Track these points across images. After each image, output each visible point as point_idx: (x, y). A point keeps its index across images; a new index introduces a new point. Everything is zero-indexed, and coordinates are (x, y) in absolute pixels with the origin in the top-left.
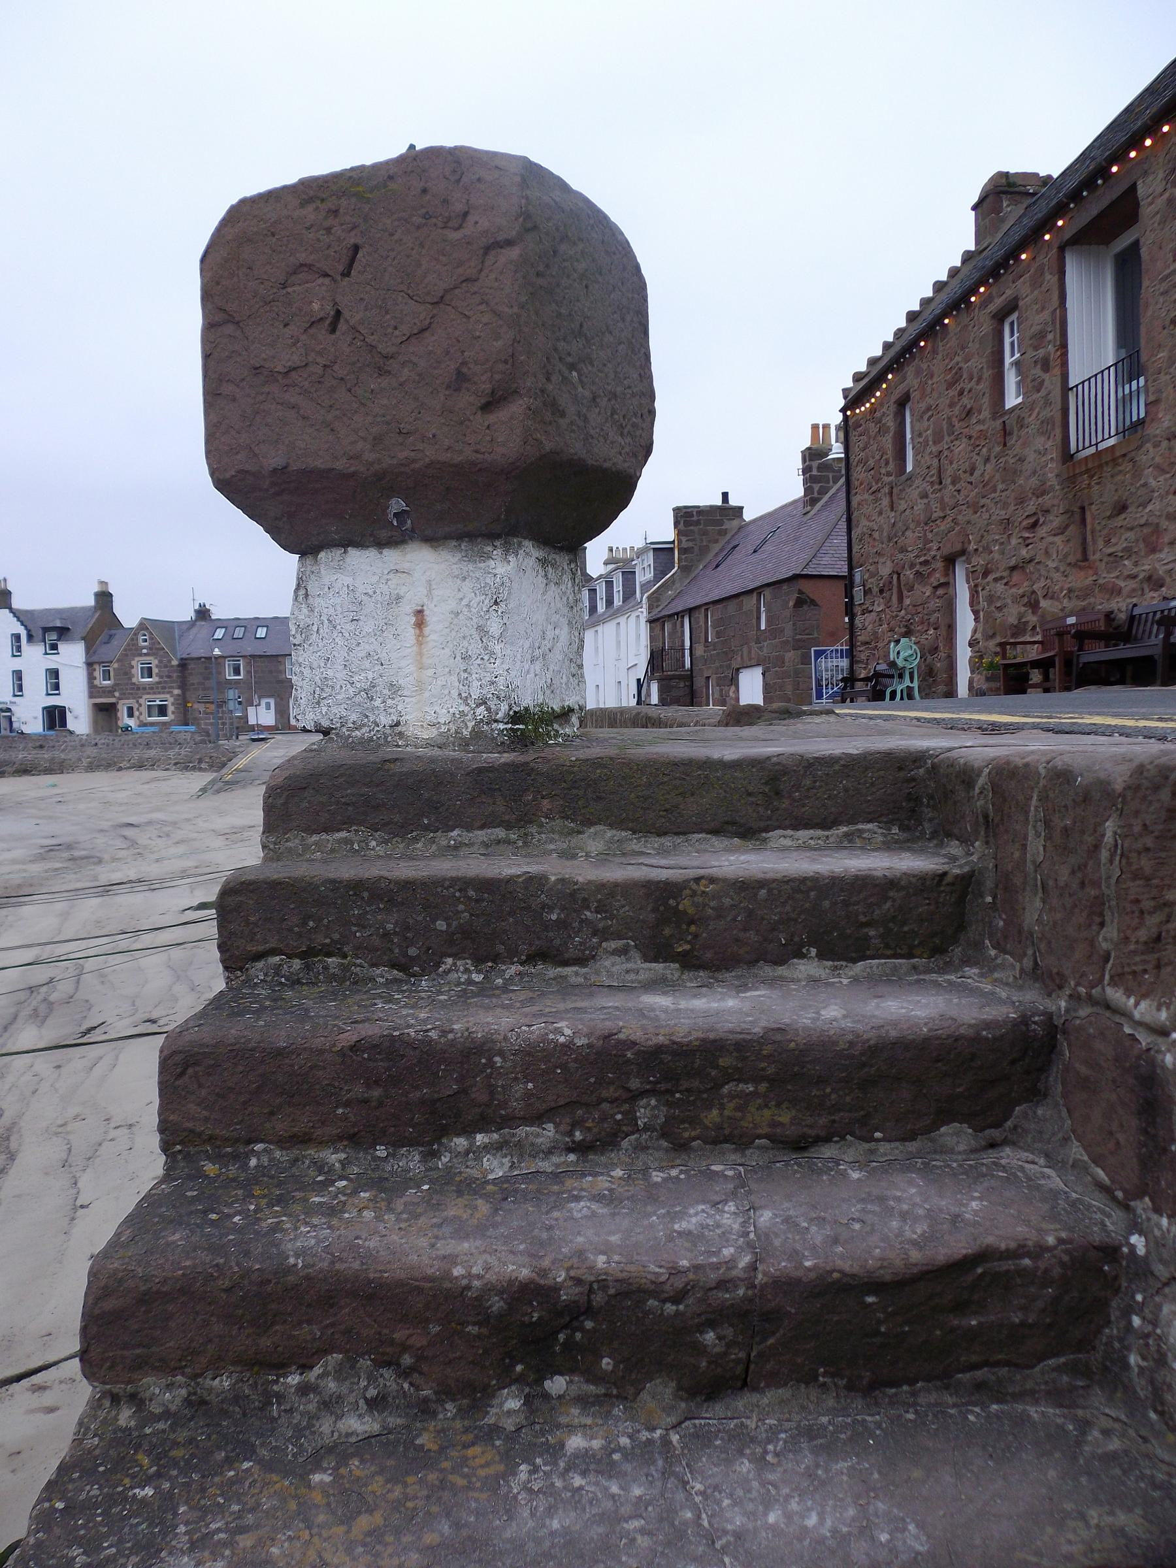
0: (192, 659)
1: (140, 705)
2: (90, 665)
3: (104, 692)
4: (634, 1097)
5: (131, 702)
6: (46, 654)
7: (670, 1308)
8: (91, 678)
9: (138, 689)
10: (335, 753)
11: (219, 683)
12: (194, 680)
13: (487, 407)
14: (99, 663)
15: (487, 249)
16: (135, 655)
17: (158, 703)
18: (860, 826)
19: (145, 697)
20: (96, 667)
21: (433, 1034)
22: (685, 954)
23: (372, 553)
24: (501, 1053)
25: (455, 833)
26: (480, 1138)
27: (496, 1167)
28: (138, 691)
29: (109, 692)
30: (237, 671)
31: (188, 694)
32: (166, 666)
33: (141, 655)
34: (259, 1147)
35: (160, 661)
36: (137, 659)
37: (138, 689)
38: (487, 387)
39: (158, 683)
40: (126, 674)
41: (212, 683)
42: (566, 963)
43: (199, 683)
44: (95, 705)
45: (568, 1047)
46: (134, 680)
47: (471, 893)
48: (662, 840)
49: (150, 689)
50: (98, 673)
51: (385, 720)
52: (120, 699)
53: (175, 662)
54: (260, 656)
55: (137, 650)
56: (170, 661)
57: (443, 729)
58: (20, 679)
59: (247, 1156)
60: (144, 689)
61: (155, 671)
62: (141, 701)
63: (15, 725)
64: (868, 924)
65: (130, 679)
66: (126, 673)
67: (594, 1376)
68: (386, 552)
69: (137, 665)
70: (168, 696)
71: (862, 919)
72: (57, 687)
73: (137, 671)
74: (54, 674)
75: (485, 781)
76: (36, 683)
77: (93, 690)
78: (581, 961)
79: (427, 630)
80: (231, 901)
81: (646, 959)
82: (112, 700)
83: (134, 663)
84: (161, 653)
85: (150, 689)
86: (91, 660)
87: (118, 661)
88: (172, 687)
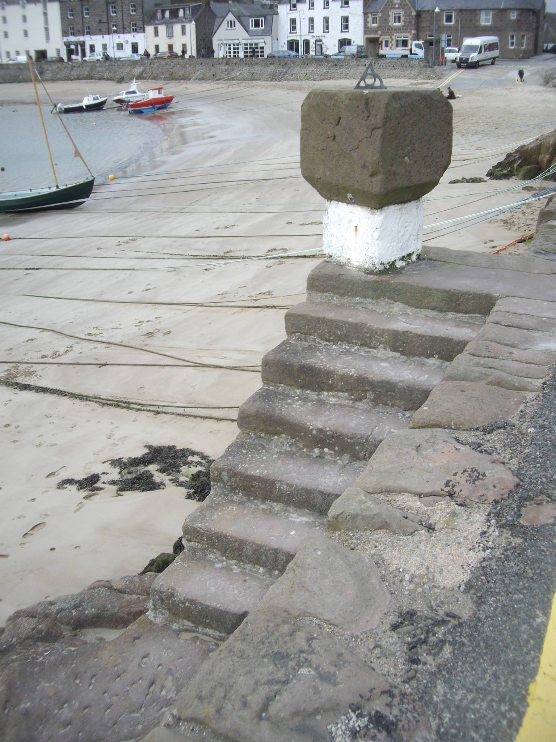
0: (424, 11)
1: (392, 40)
2: (365, 14)
3: (373, 31)
4: (366, 391)
5: (387, 38)
6: (342, 7)
7: (349, 441)
8: (366, 22)
9: (392, 29)
10: (328, 270)
11: (439, 27)
12: (424, 24)
13: (371, 176)
14: (371, 13)
15: (373, 129)
16: (391, 9)
17: (403, 38)
18: (476, 315)
19: (395, 34)
20: (369, 15)
21: (322, 367)
22: (402, 351)
23: (345, 204)
24: (336, 374)
25: (357, 298)
26: (331, 393)
27: (333, 400)
28: (392, 30)
29: (375, 31)
30: (449, 19)
31: (420, 33)
32: (408, 16)
33: (394, 8)
34: (282, 385)
35: (405, 13)
36: (392, 11)
37: (392, 29)
38: (372, 170)
39: (404, 26)
40: (385, 20)
41: (434, 27)
42: (370, 348)
43: (427, 27)
44: (367, 39)
45: (352, 376)
46: (390, 24)
47: (347, 326)
48: (416, 309)
49: (399, 30)
50: (370, 19)
51: (347, 257)
52: (381, 35)
53: (414, 13)
54: (466, 10)
55: (392, 5)
56: (411, 13)
57: (361, 264)
58: (327, 22)
59: (279, 387)
60: (395, 29)
61: (402, 18)
62: (393, 37)
63: (324, 50)
64: (452, 352)
65: (388, 23)
66: (385, 20)
67: (334, 450)
68: (349, 205)
69: (392, 14)
70: (409, 34)
71: (451, 350)
72: (347, 27)
73: (391, 19)
74: (346, 19)
75: (367, 285)
76: (335, 24)
77: (366, 29)
78: (374, 348)
79: (358, 233)
80: (288, 318)
81: (391, 350)
82: (376, 36)
83: (390, 13)
84: (406, 7)
85: (399, 30)
86: (366, 12)
87: (381, 12)
88: (411, 29)
